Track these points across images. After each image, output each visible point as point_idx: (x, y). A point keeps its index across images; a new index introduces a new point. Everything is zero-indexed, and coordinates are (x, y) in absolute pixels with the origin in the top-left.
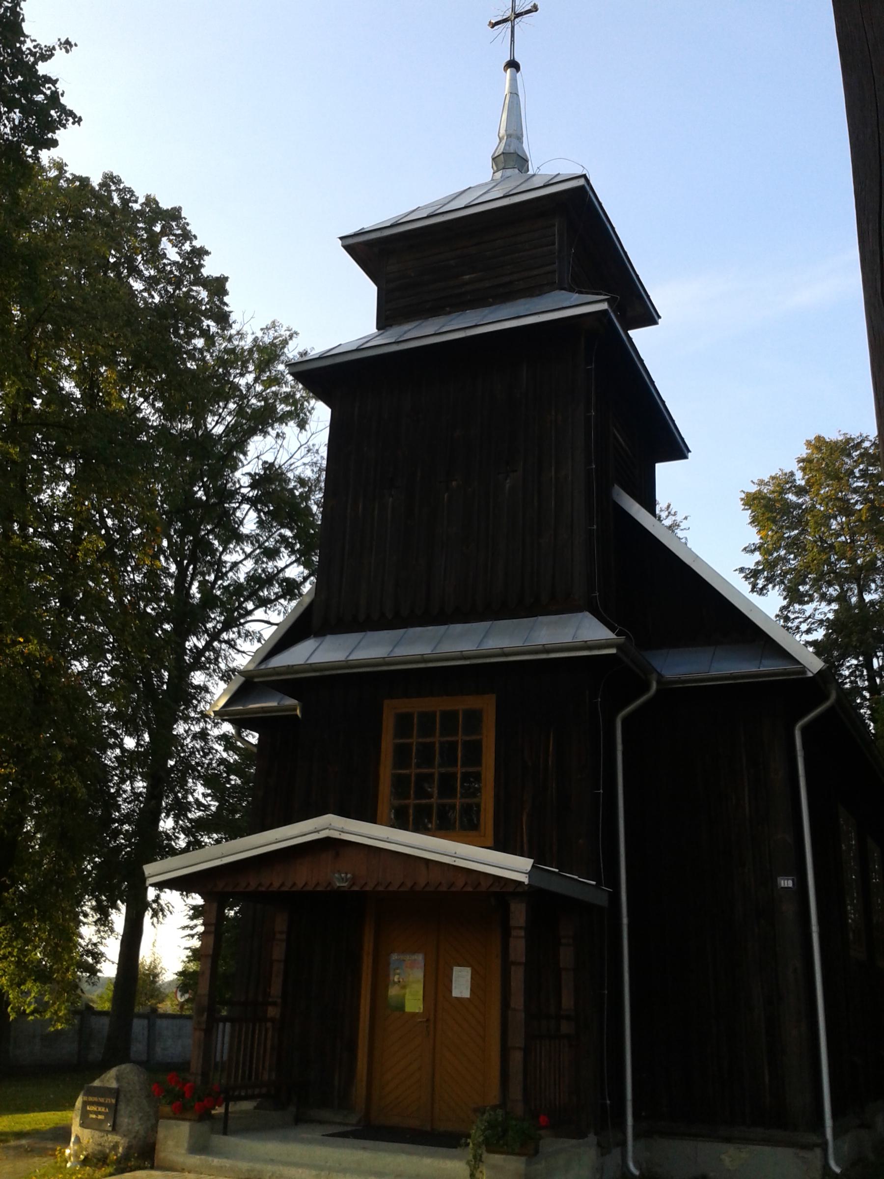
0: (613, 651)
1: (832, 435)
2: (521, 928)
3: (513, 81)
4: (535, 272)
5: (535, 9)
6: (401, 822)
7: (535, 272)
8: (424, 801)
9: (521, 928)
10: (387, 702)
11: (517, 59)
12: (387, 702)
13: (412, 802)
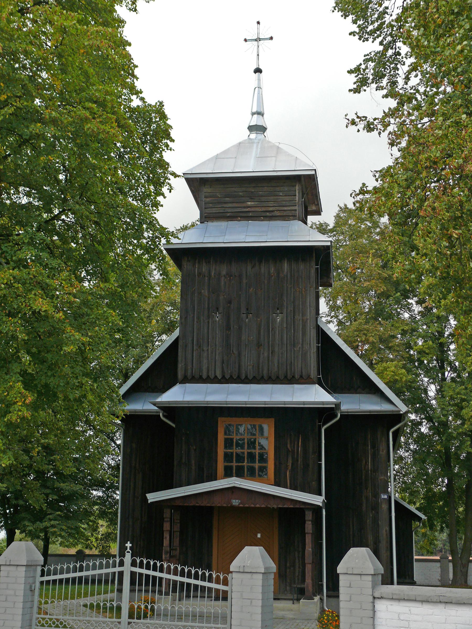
0: (334, 406)
1: (167, 110)
2: (309, 520)
3: (259, 80)
4: (285, 208)
5: (347, 127)
6: (294, 487)
7: (285, 208)
8: (240, 464)
9: (309, 520)
10: (219, 419)
11: (260, 67)
12: (219, 419)
13: (234, 464)
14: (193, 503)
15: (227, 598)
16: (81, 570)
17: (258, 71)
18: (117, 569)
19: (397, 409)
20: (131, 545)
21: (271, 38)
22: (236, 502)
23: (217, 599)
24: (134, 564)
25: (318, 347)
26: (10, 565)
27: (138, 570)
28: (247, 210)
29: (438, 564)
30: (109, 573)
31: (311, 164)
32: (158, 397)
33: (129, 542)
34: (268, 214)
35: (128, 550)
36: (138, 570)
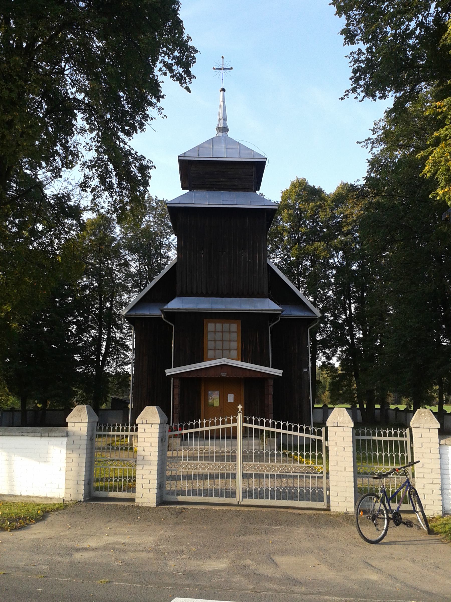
14: (186, 376)
15: (236, 437)
16: (197, 426)
17: (223, 90)
18: (231, 425)
19: (314, 315)
20: (242, 407)
21: (232, 68)
22: (224, 374)
23: (207, 438)
24: (245, 421)
25: (268, 274)
26: (146, 424)
27: (248, 425)
28: (221, 183)
29: (321, 410)
30: (219, 429)
31: (263, 155)
32: (165, 305)
33: (240, 405)
34: (234, 187)
35: (240, 410)
36: (248, 425)
